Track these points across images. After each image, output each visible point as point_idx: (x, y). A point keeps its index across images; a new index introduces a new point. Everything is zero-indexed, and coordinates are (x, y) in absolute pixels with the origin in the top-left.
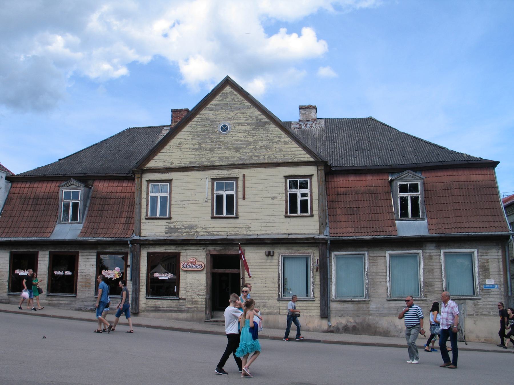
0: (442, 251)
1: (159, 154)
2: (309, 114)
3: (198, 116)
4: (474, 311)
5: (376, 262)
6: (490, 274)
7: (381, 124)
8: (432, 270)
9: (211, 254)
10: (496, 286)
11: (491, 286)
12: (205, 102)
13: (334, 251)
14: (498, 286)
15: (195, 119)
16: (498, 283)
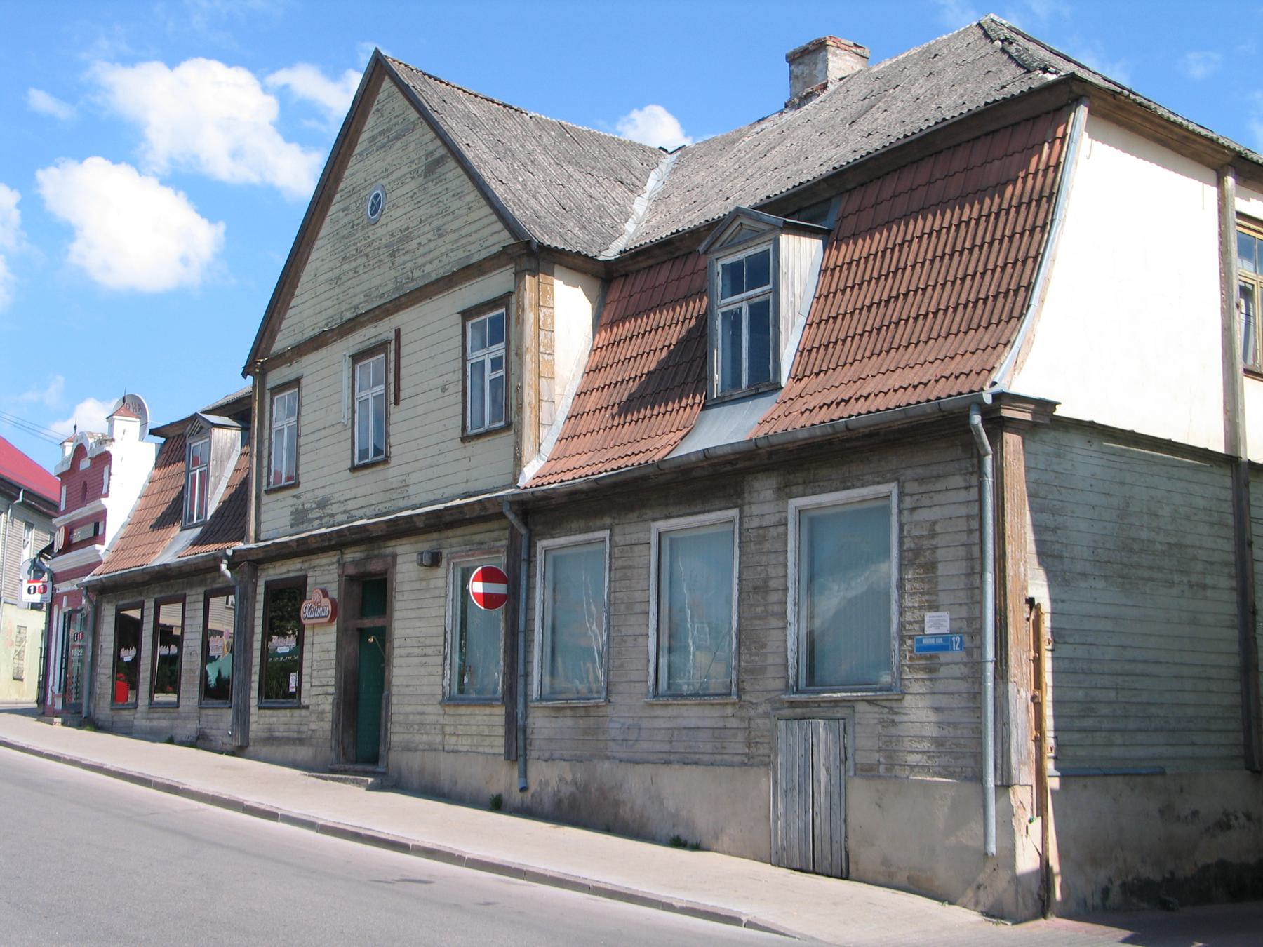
0: (795, 503)
1: (290, 313)
2: (811, 73)
3: (342, 186)
4: (879, 750)
5: (630, 567)
6: (940, 588)
7: (426, 77)
8: (766, 581)
9: (346, 576)
10: (958, 639)
11: (940, 641)
12: (347, 141)
13: (544, 536)
14: (966, 638)
15: (337, 197)
16: (964, 624)
